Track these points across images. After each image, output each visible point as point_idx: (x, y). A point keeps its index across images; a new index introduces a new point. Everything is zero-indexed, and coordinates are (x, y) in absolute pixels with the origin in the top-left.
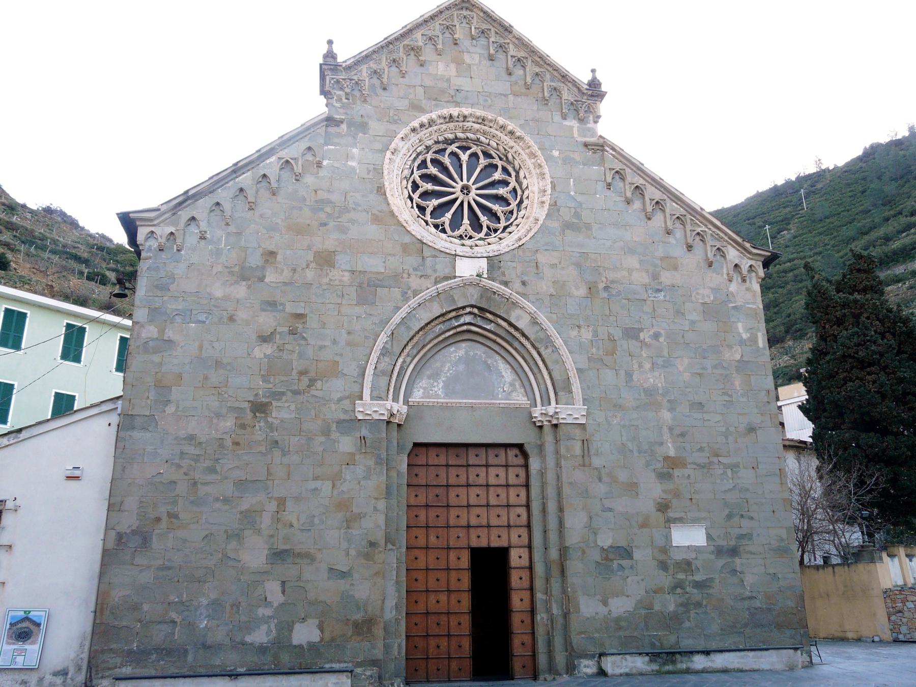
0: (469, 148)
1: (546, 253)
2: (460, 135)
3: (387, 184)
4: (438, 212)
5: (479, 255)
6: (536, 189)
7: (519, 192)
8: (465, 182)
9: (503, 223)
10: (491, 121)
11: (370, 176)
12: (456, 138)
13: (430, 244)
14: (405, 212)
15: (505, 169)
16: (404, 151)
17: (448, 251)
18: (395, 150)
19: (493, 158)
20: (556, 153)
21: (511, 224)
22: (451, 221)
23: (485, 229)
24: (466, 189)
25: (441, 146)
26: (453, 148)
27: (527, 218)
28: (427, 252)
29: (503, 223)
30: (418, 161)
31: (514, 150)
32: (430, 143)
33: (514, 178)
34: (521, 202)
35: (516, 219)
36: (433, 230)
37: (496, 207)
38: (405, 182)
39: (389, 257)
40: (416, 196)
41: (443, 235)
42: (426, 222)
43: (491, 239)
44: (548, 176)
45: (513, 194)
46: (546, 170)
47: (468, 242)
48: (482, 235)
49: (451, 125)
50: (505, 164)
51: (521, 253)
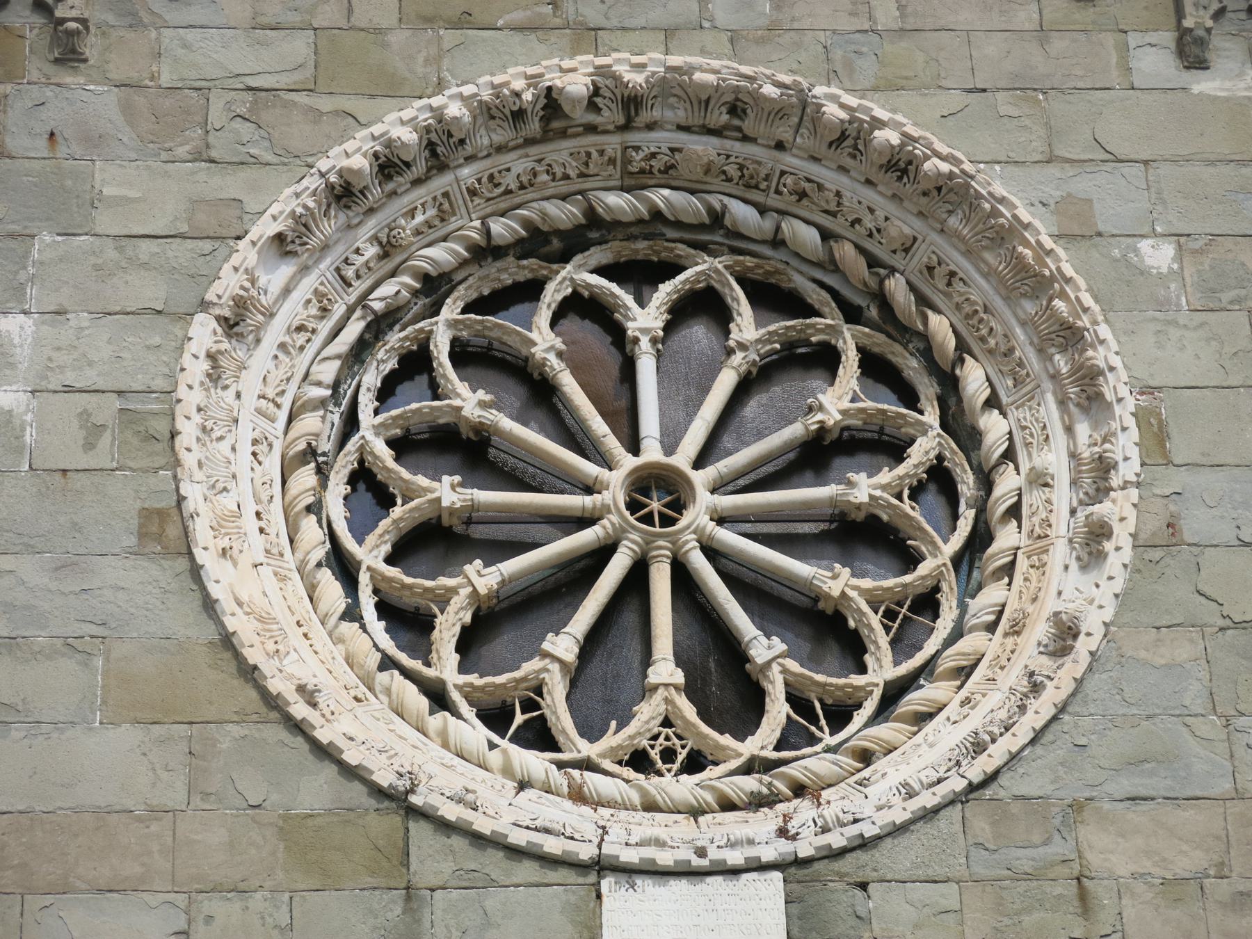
0: (672, 270)
1: (1137, 815)
2: (616, 202)
3: (193, 493)
4: (501, 643)
5: (735, 857)
6: (1054, 460)
7: (967, 485)
8: (652, 452)
9: (882, 668)
10: (778, 112)
11: (103, 456)
12: (593, 219)
13: (451, 812)
14: (314, 649)
15: (876, 368)
16: (293, 310)
17: (552, 846)
18: (241, 304)
19: (806, 310)
20: (1158, 255)
21: (927, 669)
22: (576, 677)
23: (778, 711)
24: (659, 493)
25: (509, 272)
26: (579, 274)
27: (1016, 630)
28: (431, 857)
29: (882, 668)
30: (383, 361)
31: (921, 256)
32: (441, 255)
33: (931, 416)
34: (980, 539)
35: (957, 634)
36: (475, 733)
37: (836, 580)
38: (305, 477)
39: (213, 905)
40: (371, 554)
41: (535, 762)
42: (438, 698)
43: (813, 763)
44: (1115, 386)
45: (932, 497)
46: (1107, 351)
47: (676, 786)
48: (762, 742)
49: (560, 153)
50: (879, 342)
51: (981, 826)
